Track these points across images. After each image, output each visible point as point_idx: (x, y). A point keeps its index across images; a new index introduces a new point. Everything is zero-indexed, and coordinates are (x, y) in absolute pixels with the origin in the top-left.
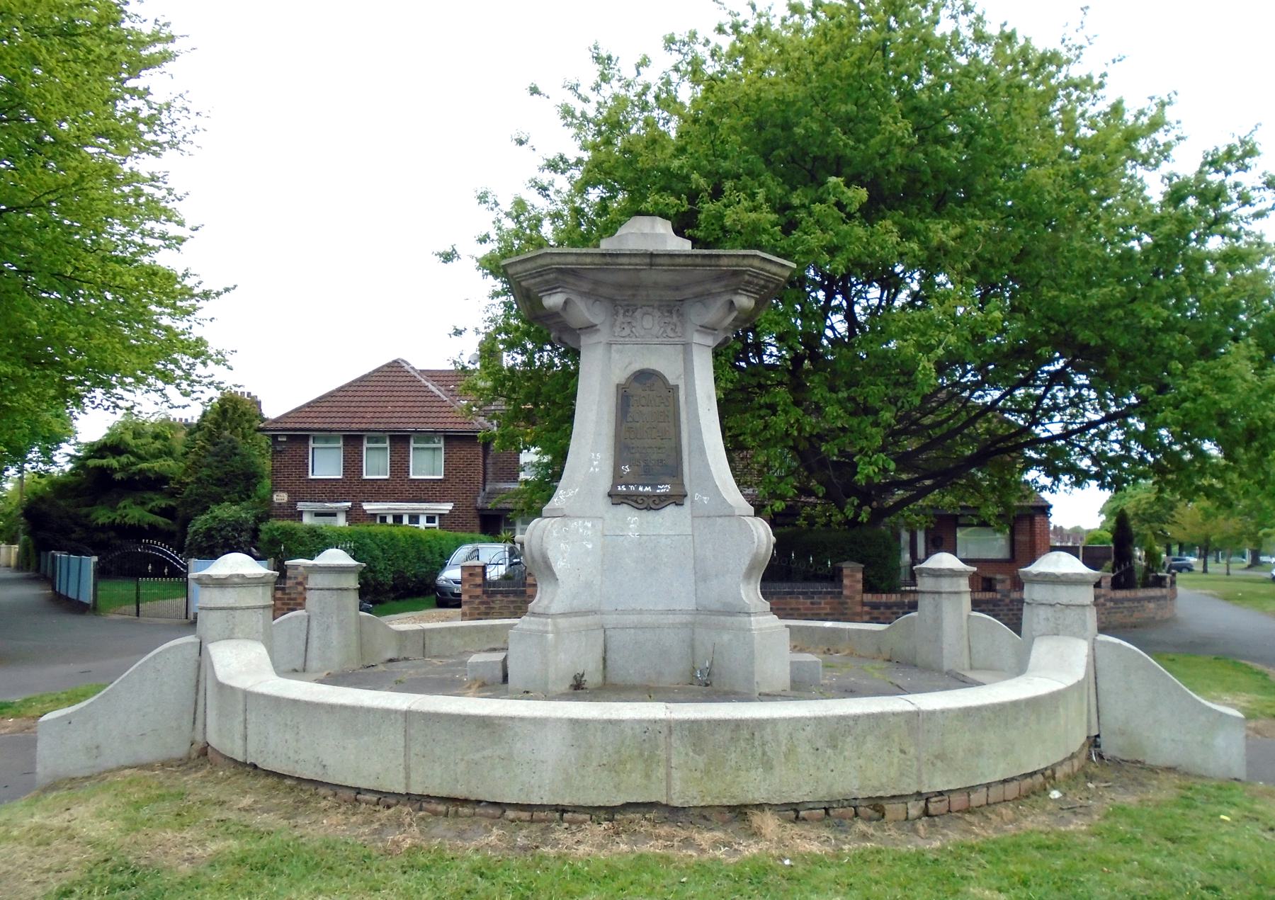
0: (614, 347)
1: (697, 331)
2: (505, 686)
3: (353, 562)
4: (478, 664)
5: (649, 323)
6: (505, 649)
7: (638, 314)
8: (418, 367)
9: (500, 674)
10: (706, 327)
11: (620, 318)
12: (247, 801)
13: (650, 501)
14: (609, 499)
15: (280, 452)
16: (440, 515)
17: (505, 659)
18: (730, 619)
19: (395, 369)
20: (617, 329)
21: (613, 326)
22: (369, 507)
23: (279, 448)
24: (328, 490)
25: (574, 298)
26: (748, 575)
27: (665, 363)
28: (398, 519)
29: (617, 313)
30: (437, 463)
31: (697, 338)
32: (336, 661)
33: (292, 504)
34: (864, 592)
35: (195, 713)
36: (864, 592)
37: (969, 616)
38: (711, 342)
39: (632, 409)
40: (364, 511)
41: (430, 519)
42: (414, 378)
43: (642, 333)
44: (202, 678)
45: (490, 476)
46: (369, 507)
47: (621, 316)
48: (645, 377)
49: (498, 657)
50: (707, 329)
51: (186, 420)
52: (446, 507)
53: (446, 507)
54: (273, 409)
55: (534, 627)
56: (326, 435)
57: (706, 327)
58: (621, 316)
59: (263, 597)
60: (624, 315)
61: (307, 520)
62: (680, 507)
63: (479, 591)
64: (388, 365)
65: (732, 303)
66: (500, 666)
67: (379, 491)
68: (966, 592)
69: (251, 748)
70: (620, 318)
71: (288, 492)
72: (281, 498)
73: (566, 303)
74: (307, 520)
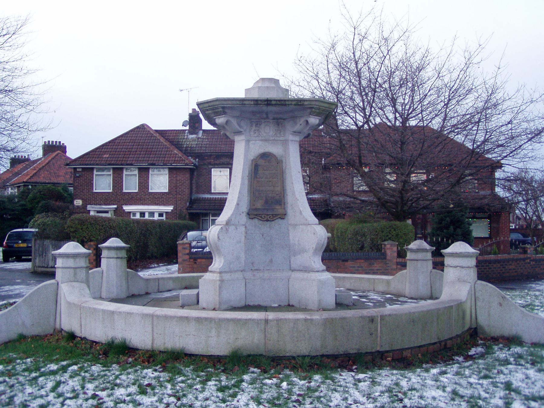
0: (251, 142)
1: (291, 134)
2: (198, 306)
3: (123, 245)
4: (184, 295)
5: (268, 130)
6: (197, 287)
7: (262, 126)
8: (154, 127)
9: (196, 301)
10: (295, 132)
11: (254, 128)
12: (362, 146)
13: (268, 217)
14: (248, 216)
15: (78, 177)
16: (166, 212)
17: (199, 292)
18: (306, 275)
19: (142, 129)
20: (252, 133)
21: (250, 131)
22: (127, 208)
23: (78, 175)
24: (105, 198)
25: (231, 119)
26: (315, 252)
27: (275, 150)
28: (142, 214)
29: (252, 126)
30: (163, 188)
31: (291, 137)
32: (115, 292)
33: (84, 206)
34: (397, 257)
35: (56, 315)
36: (397, 257)
37: (431, 272)
38: (298, 138)
39: (259, 172)
40: (124, 210)
41: (161, 215)
42: (152, 136)
43: (265, 134)
44: (59, 300)
45: (194, 190)
46: (127, 208)
47: (254, 127)
48: (265, 156)
49: (195, 292)
50: (295, 133)
51: (25, 157)
52: (170, 208)
53: (170, 208)
54: (73, 153)
55: (211, 278)
56: (104, 165)
57: (295, 132)
58: (254, 127)
59: (83, 263)
60: (256, 126)
61: (92, 213)
62: (283, 220)
63: (187, 257)
64: (138, 128)
65: (307, 122)
66: (196, 296)
67: (133, 199)
68: (429, 260)
69: (83, 332)
70: (254, 128)
71: (82, 199)
72: (78, 202)
73: (227, 122)
74: (92, 213)
